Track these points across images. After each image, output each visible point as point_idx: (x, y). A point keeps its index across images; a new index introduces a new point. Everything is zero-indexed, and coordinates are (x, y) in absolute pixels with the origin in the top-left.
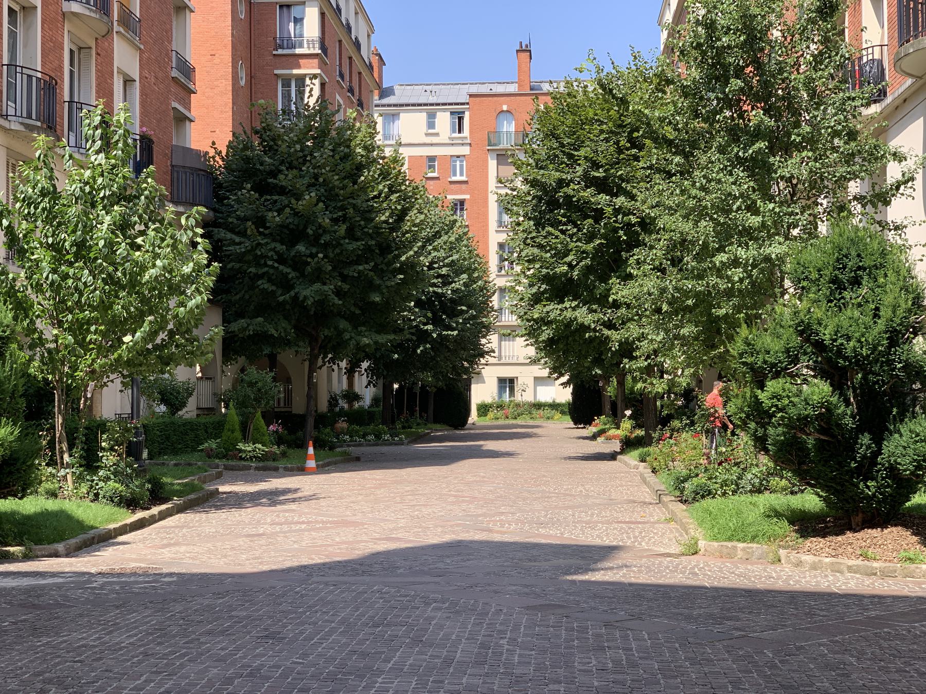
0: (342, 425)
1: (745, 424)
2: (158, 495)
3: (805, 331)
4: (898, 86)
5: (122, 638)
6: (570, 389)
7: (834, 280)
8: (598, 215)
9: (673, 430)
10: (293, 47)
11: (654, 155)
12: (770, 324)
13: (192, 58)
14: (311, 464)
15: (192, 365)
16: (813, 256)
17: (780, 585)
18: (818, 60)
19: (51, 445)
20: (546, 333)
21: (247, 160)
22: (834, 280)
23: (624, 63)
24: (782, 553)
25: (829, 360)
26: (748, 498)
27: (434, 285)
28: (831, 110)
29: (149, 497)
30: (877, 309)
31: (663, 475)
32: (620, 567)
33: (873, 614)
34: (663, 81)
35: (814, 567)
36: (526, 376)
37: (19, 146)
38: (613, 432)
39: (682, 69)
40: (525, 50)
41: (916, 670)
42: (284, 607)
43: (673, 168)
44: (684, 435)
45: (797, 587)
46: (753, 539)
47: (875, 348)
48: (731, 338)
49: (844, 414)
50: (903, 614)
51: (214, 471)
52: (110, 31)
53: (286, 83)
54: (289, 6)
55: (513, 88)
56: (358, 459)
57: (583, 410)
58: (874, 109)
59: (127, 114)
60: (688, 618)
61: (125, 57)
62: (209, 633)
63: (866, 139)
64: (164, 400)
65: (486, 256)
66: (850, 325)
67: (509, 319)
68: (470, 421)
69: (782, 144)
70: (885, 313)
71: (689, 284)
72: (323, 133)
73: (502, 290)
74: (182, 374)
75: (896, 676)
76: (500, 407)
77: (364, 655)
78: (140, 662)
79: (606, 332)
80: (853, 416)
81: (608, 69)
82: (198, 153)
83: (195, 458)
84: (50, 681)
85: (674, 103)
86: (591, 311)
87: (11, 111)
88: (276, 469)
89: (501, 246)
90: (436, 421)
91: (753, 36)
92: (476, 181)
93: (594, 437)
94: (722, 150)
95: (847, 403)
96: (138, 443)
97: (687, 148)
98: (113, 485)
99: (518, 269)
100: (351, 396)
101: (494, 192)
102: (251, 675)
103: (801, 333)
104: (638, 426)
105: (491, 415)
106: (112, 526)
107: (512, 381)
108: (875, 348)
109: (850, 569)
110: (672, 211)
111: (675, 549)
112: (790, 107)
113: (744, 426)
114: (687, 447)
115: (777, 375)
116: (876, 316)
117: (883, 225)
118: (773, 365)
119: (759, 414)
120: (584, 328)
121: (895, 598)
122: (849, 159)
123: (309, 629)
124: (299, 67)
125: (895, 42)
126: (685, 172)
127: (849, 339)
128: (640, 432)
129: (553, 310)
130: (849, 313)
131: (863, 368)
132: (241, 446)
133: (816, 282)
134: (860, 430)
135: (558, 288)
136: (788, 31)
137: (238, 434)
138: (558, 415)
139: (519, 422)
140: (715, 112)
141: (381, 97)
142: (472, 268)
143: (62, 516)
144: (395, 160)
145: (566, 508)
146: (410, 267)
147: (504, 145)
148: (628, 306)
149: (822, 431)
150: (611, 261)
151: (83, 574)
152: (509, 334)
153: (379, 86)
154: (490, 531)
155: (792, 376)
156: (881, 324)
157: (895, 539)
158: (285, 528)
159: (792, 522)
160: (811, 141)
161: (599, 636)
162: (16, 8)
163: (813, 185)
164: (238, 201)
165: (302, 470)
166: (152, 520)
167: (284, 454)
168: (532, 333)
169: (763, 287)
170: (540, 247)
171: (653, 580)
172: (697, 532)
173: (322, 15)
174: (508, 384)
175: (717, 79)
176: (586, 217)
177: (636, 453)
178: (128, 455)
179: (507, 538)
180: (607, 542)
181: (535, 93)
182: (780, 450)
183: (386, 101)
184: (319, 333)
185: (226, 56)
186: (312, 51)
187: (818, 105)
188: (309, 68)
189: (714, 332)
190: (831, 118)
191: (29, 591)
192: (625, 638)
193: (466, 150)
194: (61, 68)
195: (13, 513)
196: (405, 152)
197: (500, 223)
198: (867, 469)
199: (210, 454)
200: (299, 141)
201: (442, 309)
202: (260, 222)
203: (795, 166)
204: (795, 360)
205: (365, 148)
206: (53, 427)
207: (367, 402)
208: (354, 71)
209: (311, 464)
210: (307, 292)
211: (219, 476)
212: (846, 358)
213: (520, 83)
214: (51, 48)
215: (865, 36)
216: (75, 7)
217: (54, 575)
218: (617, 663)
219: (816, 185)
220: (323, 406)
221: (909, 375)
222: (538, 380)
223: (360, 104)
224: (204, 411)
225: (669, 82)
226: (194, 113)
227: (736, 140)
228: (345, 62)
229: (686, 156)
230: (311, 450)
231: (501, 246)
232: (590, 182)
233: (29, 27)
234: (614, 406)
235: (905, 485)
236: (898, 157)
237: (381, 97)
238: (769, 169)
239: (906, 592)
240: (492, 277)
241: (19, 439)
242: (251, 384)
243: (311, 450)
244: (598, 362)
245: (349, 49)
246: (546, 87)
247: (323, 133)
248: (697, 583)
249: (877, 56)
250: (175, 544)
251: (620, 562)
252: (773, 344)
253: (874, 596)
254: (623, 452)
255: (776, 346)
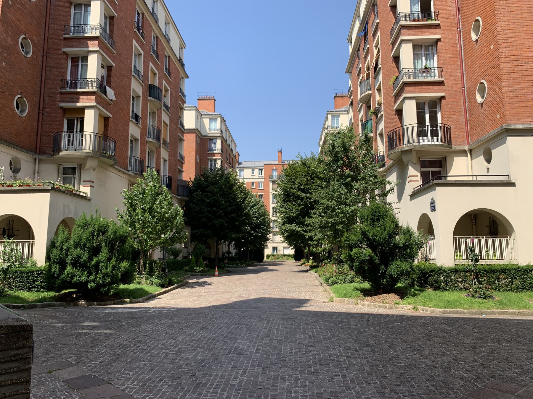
0: (226, 261)
1: (347, 262)
2: (170, 284)
3: (364, 234)
4: (389, 163)
5: (159, 328)
6: (294, 250)
7: (372, 219)
8: (302, 199)
9: (325, 263)
10: (213, 151)
11: (319, 182)
12: (353, 232)
13: (185, 154)
14: (217, 273)
15: (181, 243)
16: (365, 212)
17: (358, 311)
18: (365, 155)
19: (139, 268)
20: (286, 234)
21: (199, 183)
22: (372, 219)
23: (309, 155)
24: (359, 301)
25: (370, 243)
26: (348, 285)
27: (254, 220)
28: (369, 170)
29: (167, 284)
30: (385, 228)
31: (323, 277)
32: (310, 306)
33: (386, 320)
34: (320, 161)
35: (368, 306)
36: (281, 246)
37: (132, 179)
38: (307, 264)
39: (325, 158)
40: (280, 152)
41: (400, 338)
42: (208, 318)
43: (324, 186)
44: (328, 265)
45: (363, 312)
46: (350, 297)
47: (384, 239)
48: (342, 236)
49: (376, 259)
50: (395, 320)
51: (187, 276)
52: (160, 147)
53: (211, 161)
54: (212, 139)
55: (277, 163)
56: (231, 272)
57: (298, 257)
58: (382, 169)
59: (165, 171)
60: (331, 322)
61: (164, 154)
62: (186, 326)
63: (380, 178)
64: (173, 254)
65: (269, 211)
66: (377, 232)
67: (276, 229)
68: (264, 260)
69: (355, 179)
70: (387, 229)
71: (330, 220)
72: (222, 175)
73: (274, 221)
74: (178, 246)
75: (394, 340)
76: (273, 256)
77: (233, 334)
78: (165, 336)
79: (305, 234)
80: (379, 260)
81: (304, 157)
82: (185, 181)
83: (182, 272)
84: (137, 342)
85: (324, 167)
86: (299, 227)
87: (130, 169)
88: (206, 275)
89: (273, 208)
90: (254, 260)
91: (346, 149)
92: (266, 190)
93: (301, 265)
94: (338, 181)
95: (377, 256)
96: (165, 267)
97: (328, 180)
98: (157, 280)
99: (278, 215)
100: (229, 252)
101: (271, 192)
102: (198, 340)
103: (363, 235)
104: (314, 262)
105: (270, 258)
106: (156, 293)
107: (276, 248)
108: (384, 239)
109: (379, 306)
110: (323, 198)
111: (326, 300)
112: (357, 169)
113: (346, 262)
114: (330, 268)
115: (356, 247)
116: (385, 230)
117: (386, 203)
118: (355, 244)
119: (351, 259)
120: (297, 232)
121: (393, 315)
122: (375, 184)
123: (216, 326)
124: (215, 156)
125: (388, 150)
126: (327, 187)
127: (377, 236)
128: (315, 264)
129: (288, 226)
130: (376, 229)
131: (381, 245)
132: (195, 268)
133: (367, 219)
134: (381, 264)
135: (290, 220)
136: (356, 147)
137: (195, 264)
138: (290, 258)
139: (279, 260)
140: (335, 170)
141: (239, 165)
142: (264, 215)
143: (141, 289)
144: (243, 183)
145: (293, 287)
146: (247, 214)
147: (274, 179)
148: (311, 226)
149: (369, 264)
150: (305, 212)
151: (148, 308)
152: (275, 234)
153: (238, 162)
154: (270, 294)
155: (360, 247)
156: (386, 232)
157: (392, 297)
158: (209, 294)
159: (361, 292)
160: (364, 178)
161: (304, 328)
162: (133, 139)
163: (364, 191)
164: (196, 195)
165: (214, 275)
166: (169, 291)
167: (208, 271)
168: (282, 234)
169: (351, 220)
170: (285, 208)
171: (320, 310)
172: (333, 295)
173: (222, 142)
174: (275, 249)
175: (336, 161)
176: (298, 200)
177: (314, 270)
178: (162, 271)
179: (276, 297)
180: (306, 298)
181: (283, 164)
182: (357, 270)
183: (240, 166)
184: (221, 235)
185: (194, 153)
186: (94, 35)
187: (365, 168)
188: (218, 157)
189: (337, 234)
190: (369, 172)
191: (132, 312)
192: (312, 328)
193: (263, 180)
194: (145, 157)
195: (127, 289)
196: (246, 181)
197: (273, 201)
198: (383, 275)
199: (186, 271)
200: (214, 178)
201: (257, 227)
202: (203, 201)
203: (357, 185)
204: (361, 243)
205: (234, 180)
206: (140, 263)
207: (234, 254)
208: (230, 157)
209: (217, 273)
210: (217, 222)
211: (189, 277)
212: (376, 242)
213: (279, 161)
214: (143, 151)
215: (379, 148)
216: (150, 140)
217: (139, 308)
218: (310, 336)
219: (365, 191)
220: (220, 256)
221: (395, 248)
222: (284, 248)
223: (233, 167)
224: (184, 257)
225: (322, 161)
226: (184, 170)
227: (342, 178)
228: (231, 159)
229: (328, 182)
230: (217, 269)
231: (273, 208)
232: (299, 189)
233: (136, 145)
234: (307, 255)
235: (395, 281)
236: (389, 183)
237: (239, 165)
238: (352, 186)
239: (396, 313)
240: (271, 217)
241: (129, 266)
242: (199, 249)
243: (217, 269)
244: (302, 242)
245: (229, 151)
246: (286, 162)
247: (222, 175)
248: (333, 311)
249: (382, 154)
250: (176, 299)
251: (310, 304)
252: (354, 238)
253: (386, 315)
254: (310, 270)
255: (355, 238)
